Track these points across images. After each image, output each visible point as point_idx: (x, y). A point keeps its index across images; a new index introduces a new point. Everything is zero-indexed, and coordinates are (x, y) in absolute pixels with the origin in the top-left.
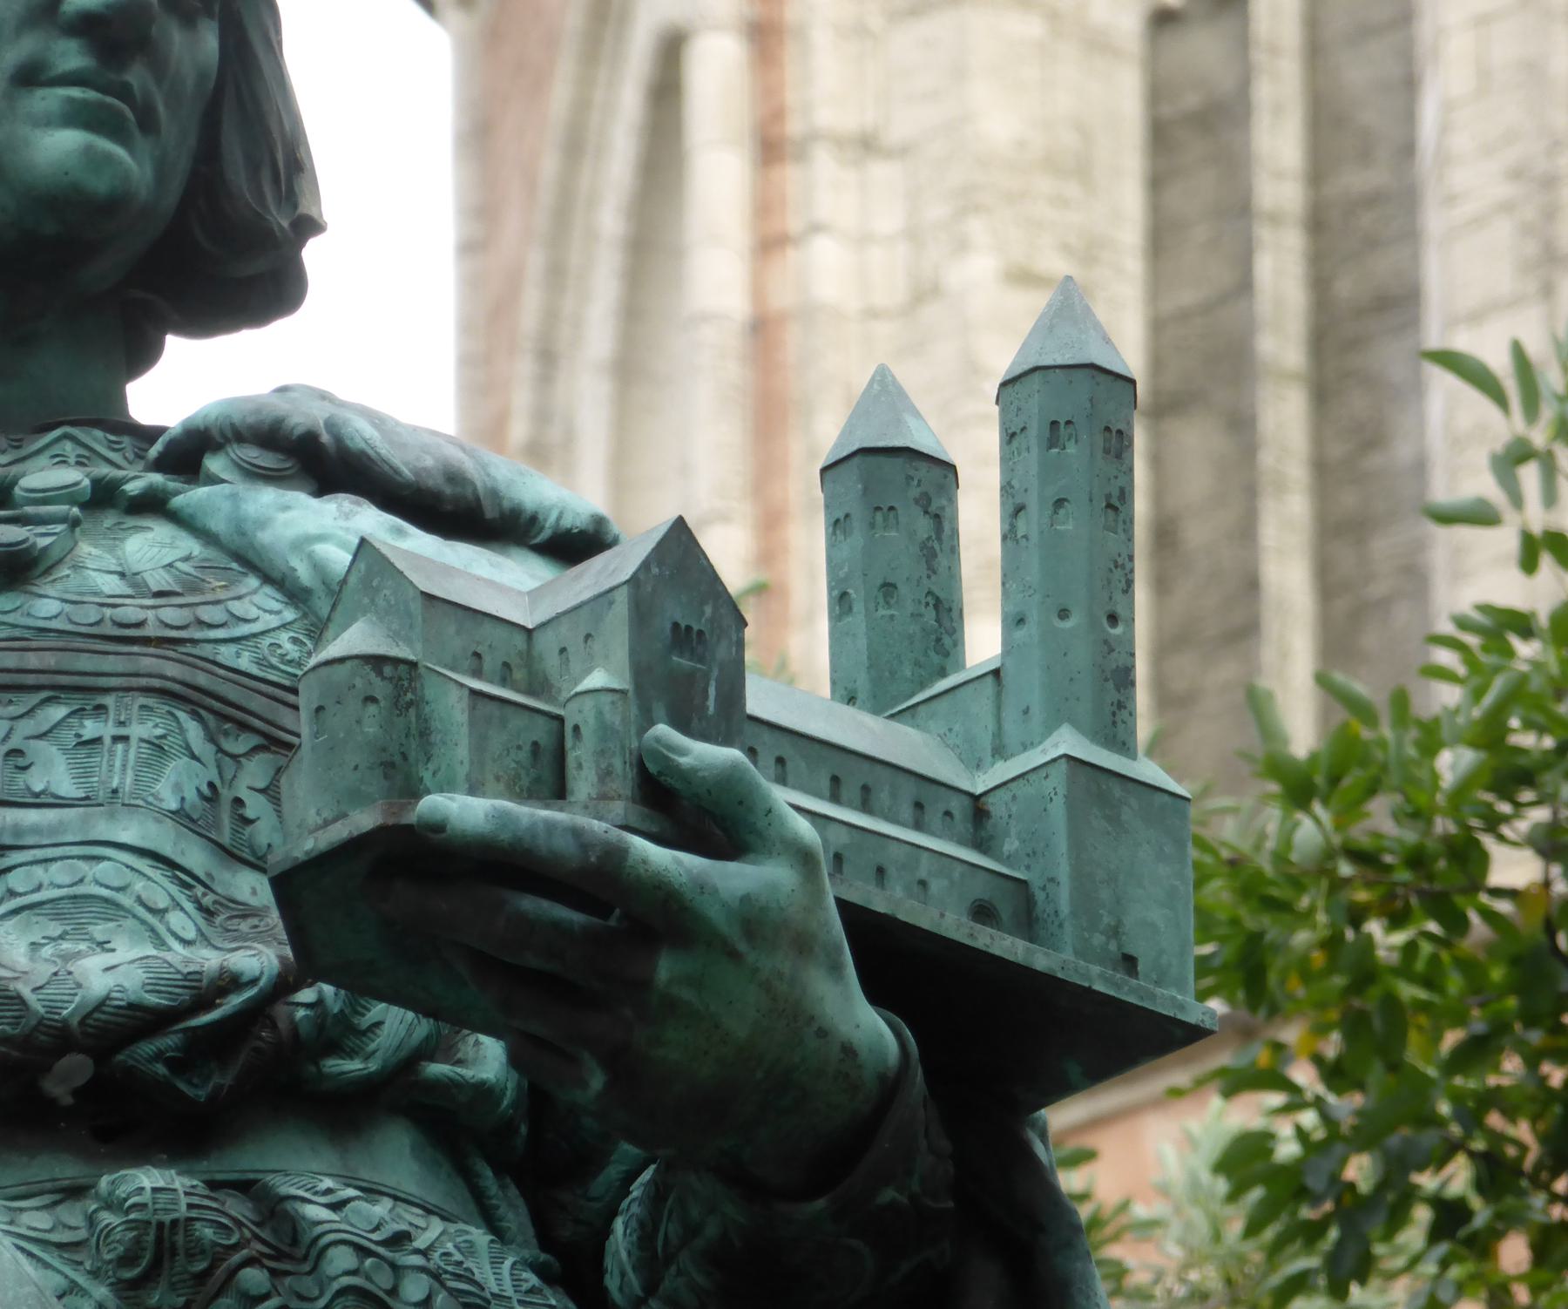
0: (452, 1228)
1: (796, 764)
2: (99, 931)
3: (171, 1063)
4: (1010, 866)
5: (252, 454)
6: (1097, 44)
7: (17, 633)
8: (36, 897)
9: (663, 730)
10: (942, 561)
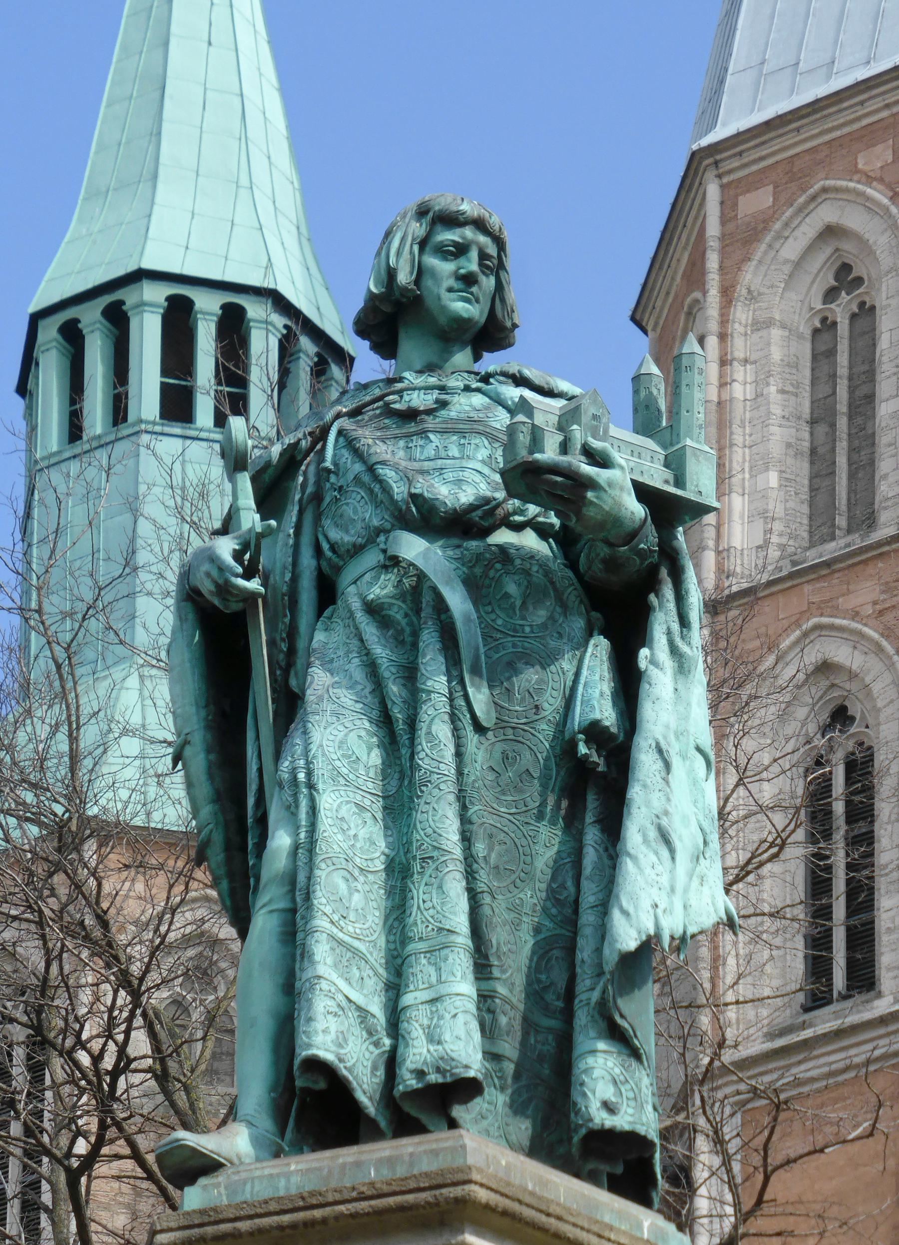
1: (623, 447)
5: (502, 378)
6: (800, 337)
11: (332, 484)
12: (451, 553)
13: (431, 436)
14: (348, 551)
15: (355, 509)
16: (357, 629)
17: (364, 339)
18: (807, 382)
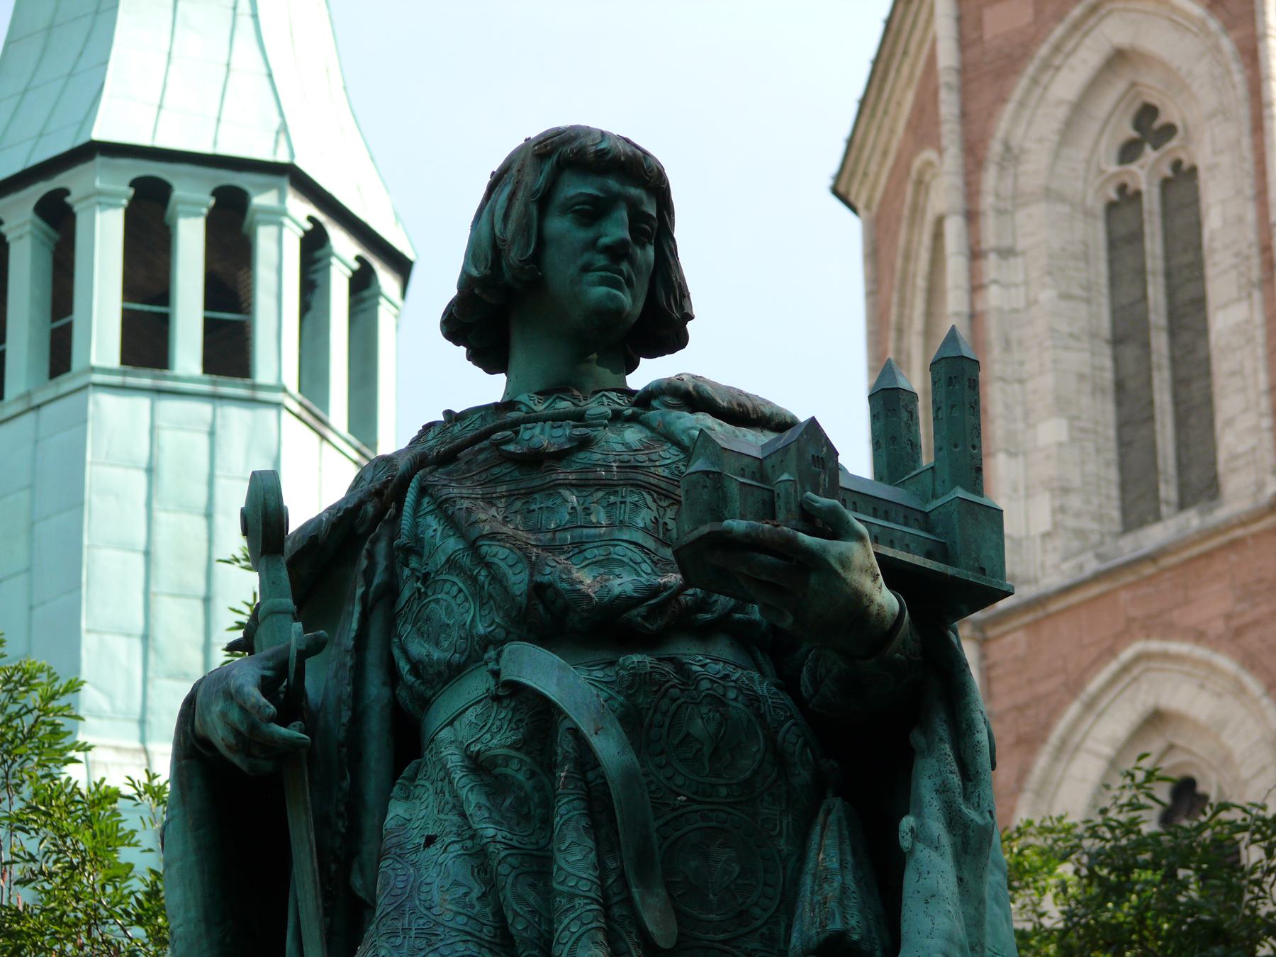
0: (745, 672)
2: (617, 571)
3: (644, 618)
4: (938, 537)
5: (668, 399)
7: (586, 466)
8: (595, 560)
9: (809, 494)
10: (913, 428)
11: (413, 570)
12: (599, 674)
13: (566, 493)
14: (439, 674)
15: (448, 608)
16: (456, 797)
17: (457, 344)
18: (1103, 280)
